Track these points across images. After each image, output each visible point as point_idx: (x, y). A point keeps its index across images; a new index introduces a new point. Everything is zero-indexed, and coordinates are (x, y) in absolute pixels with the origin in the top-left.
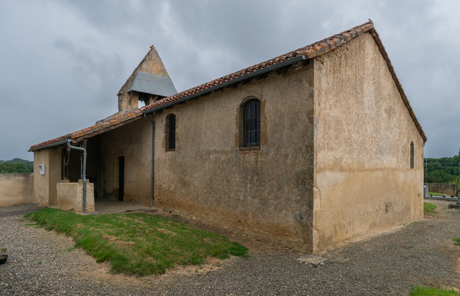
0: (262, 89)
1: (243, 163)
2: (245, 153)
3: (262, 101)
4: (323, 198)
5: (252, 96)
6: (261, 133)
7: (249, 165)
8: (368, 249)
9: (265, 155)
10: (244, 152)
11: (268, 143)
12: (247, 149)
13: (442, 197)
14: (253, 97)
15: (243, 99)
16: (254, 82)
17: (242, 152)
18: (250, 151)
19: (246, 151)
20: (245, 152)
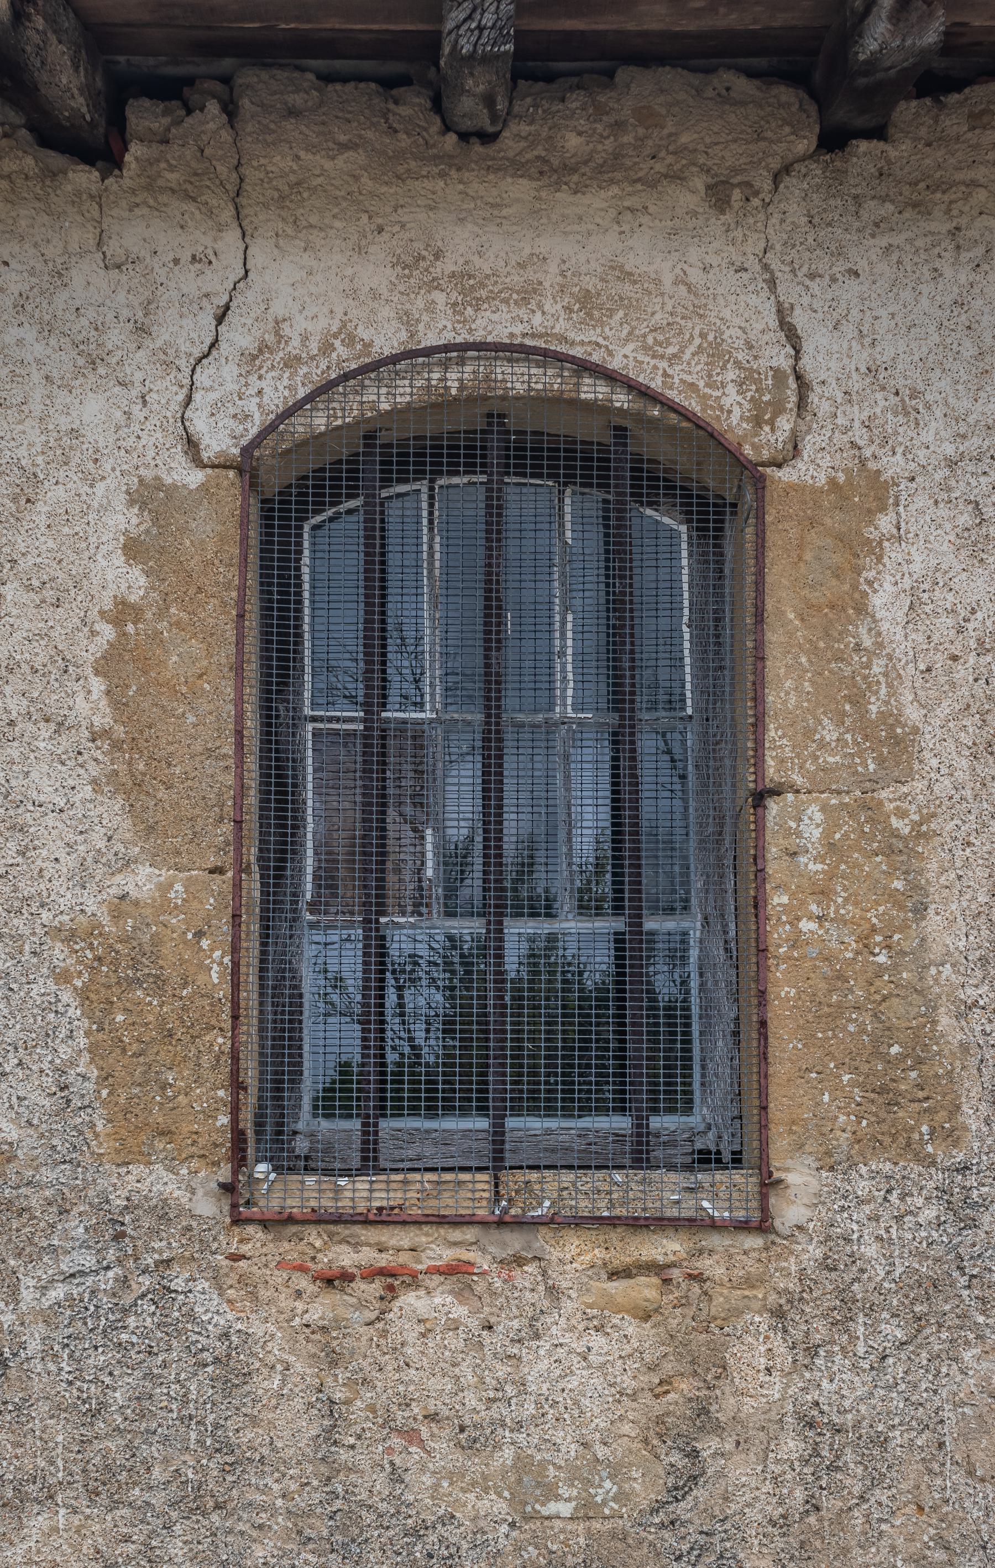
0: (788, 291)
1: (329, 1436)
2: (373, 1273)
3: (785, 475)
4: (244, 1038)
5: (547, 357)
6: (779, 972)
7: (483, 1485)
8: (549, 1371)
9: (894, 1331)
10: (346, 1258)
11: (953, 1137)
12: (448, 1204)
13: (570, 617)
14: (584, 367)
15: (317, 372)
16: (573, 142)
17: (290, 1250)
18: (515, 1242)
19: (401, 1238)
20: (367, 1256)
